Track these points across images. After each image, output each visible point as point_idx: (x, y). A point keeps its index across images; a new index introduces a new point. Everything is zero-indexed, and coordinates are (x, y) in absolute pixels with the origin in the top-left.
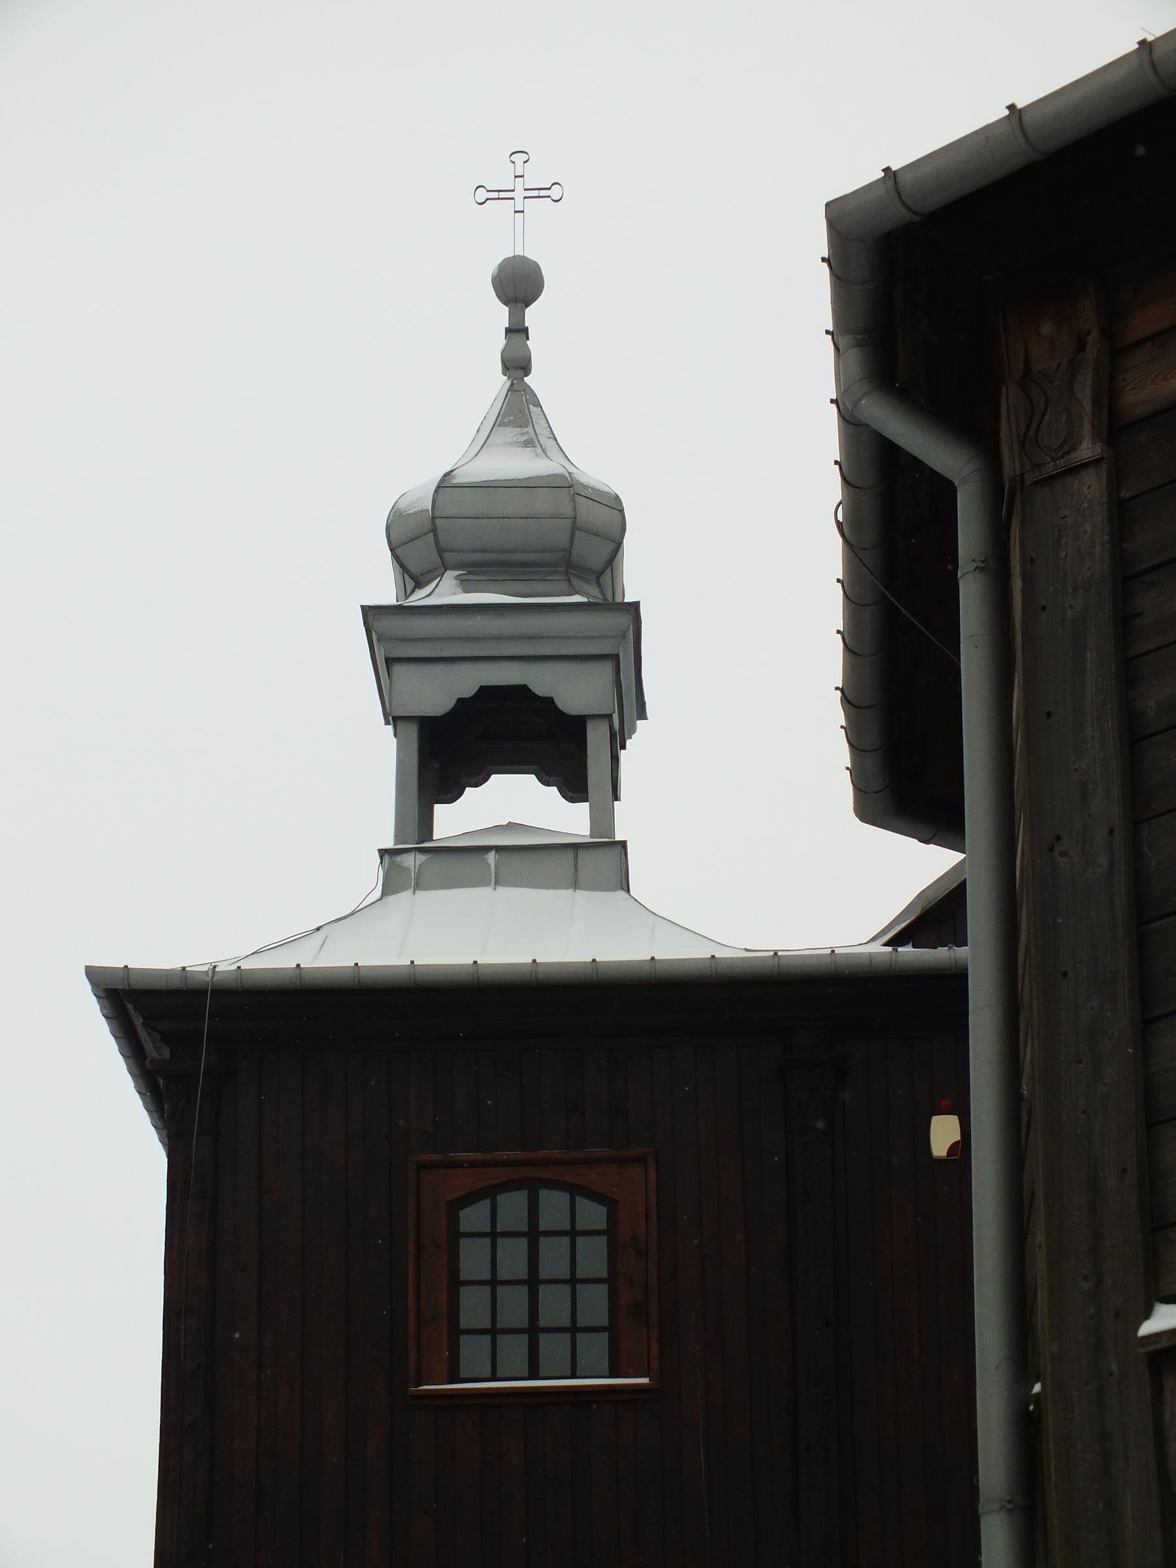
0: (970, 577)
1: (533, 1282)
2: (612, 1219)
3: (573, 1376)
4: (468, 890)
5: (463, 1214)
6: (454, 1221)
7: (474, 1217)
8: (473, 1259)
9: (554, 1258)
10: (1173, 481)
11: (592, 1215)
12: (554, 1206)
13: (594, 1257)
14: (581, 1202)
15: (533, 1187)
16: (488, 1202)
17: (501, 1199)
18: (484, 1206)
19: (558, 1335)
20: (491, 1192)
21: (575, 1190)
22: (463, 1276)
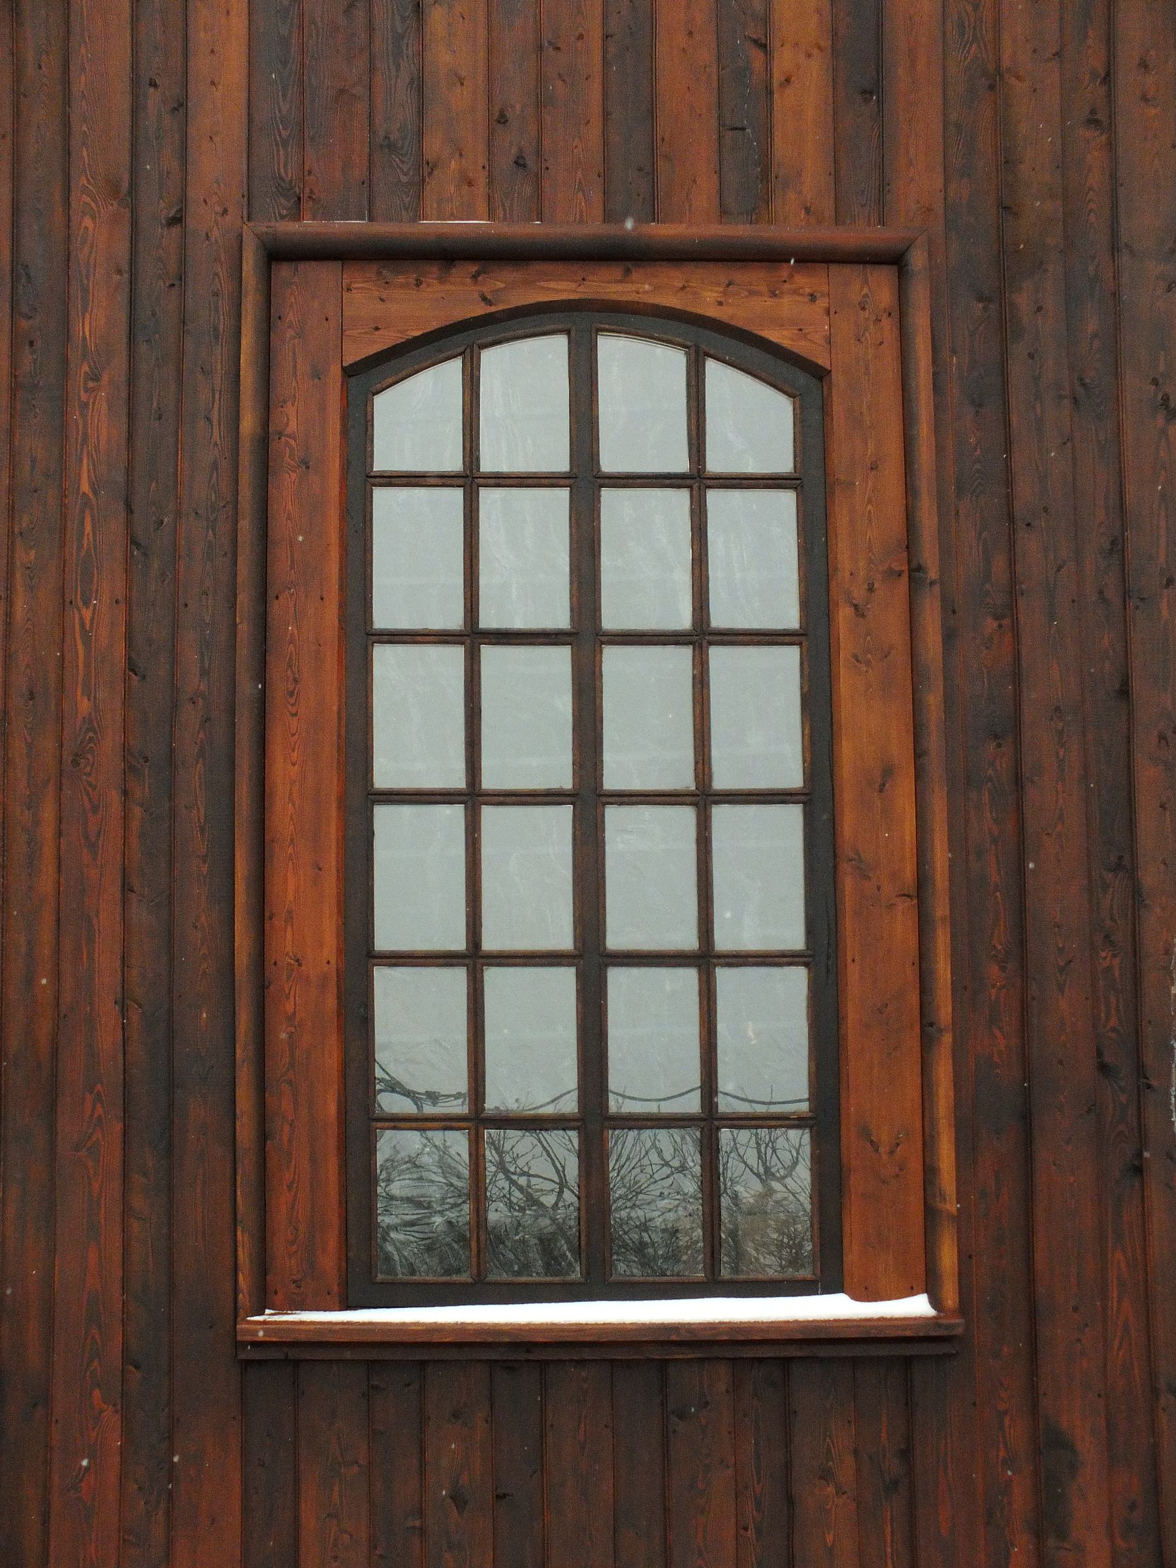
0: (916, 269)
1: (585, 637)
2: (813, 435)
3: (827, 1281)
4: (695, 892)
5: (383, 404)
6: (358, 430)
7: (414, 419)
8: (411, 557)
9: (644, 552)
10: (297, 1561)
11: (753, 422)
12: (640, 378)
13: (759, 561)
14: (717, 374)
15: (582, 323)
16: (452, 370)
17: (493, 360)
18: (439, 383)
19: (636, 785)
20: (463, 339)
21: (706, 340)
22: (382, 619)
